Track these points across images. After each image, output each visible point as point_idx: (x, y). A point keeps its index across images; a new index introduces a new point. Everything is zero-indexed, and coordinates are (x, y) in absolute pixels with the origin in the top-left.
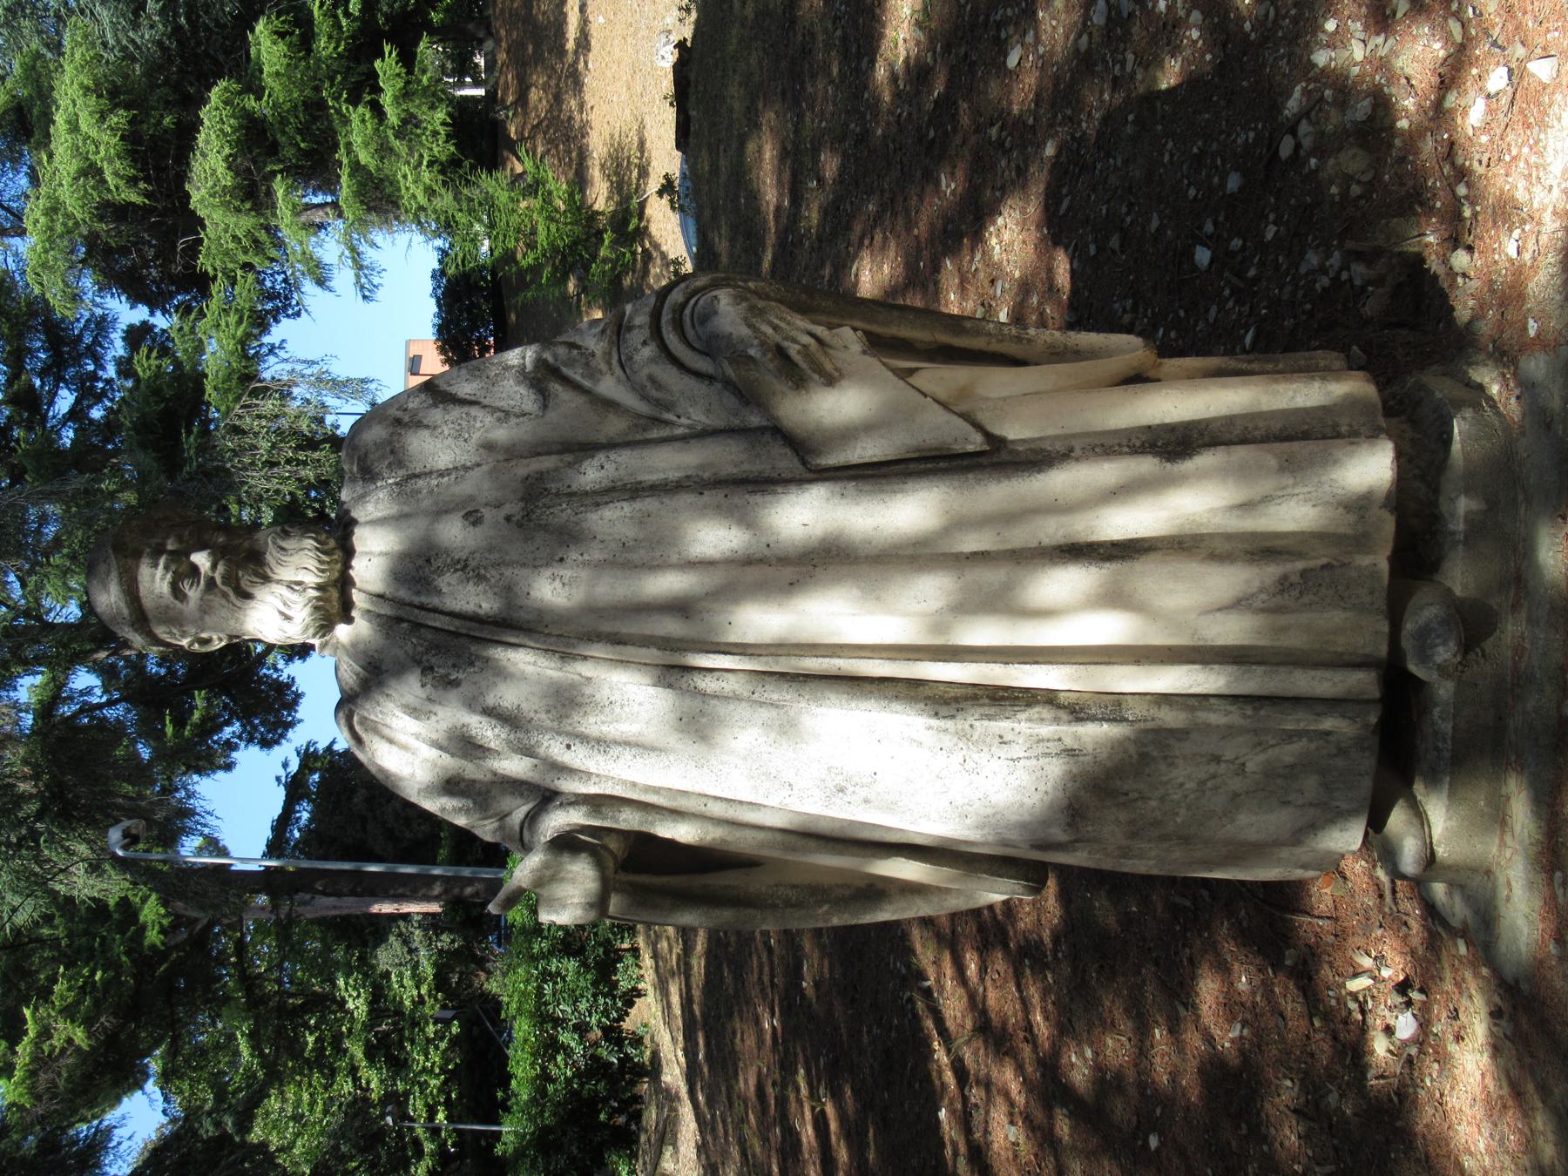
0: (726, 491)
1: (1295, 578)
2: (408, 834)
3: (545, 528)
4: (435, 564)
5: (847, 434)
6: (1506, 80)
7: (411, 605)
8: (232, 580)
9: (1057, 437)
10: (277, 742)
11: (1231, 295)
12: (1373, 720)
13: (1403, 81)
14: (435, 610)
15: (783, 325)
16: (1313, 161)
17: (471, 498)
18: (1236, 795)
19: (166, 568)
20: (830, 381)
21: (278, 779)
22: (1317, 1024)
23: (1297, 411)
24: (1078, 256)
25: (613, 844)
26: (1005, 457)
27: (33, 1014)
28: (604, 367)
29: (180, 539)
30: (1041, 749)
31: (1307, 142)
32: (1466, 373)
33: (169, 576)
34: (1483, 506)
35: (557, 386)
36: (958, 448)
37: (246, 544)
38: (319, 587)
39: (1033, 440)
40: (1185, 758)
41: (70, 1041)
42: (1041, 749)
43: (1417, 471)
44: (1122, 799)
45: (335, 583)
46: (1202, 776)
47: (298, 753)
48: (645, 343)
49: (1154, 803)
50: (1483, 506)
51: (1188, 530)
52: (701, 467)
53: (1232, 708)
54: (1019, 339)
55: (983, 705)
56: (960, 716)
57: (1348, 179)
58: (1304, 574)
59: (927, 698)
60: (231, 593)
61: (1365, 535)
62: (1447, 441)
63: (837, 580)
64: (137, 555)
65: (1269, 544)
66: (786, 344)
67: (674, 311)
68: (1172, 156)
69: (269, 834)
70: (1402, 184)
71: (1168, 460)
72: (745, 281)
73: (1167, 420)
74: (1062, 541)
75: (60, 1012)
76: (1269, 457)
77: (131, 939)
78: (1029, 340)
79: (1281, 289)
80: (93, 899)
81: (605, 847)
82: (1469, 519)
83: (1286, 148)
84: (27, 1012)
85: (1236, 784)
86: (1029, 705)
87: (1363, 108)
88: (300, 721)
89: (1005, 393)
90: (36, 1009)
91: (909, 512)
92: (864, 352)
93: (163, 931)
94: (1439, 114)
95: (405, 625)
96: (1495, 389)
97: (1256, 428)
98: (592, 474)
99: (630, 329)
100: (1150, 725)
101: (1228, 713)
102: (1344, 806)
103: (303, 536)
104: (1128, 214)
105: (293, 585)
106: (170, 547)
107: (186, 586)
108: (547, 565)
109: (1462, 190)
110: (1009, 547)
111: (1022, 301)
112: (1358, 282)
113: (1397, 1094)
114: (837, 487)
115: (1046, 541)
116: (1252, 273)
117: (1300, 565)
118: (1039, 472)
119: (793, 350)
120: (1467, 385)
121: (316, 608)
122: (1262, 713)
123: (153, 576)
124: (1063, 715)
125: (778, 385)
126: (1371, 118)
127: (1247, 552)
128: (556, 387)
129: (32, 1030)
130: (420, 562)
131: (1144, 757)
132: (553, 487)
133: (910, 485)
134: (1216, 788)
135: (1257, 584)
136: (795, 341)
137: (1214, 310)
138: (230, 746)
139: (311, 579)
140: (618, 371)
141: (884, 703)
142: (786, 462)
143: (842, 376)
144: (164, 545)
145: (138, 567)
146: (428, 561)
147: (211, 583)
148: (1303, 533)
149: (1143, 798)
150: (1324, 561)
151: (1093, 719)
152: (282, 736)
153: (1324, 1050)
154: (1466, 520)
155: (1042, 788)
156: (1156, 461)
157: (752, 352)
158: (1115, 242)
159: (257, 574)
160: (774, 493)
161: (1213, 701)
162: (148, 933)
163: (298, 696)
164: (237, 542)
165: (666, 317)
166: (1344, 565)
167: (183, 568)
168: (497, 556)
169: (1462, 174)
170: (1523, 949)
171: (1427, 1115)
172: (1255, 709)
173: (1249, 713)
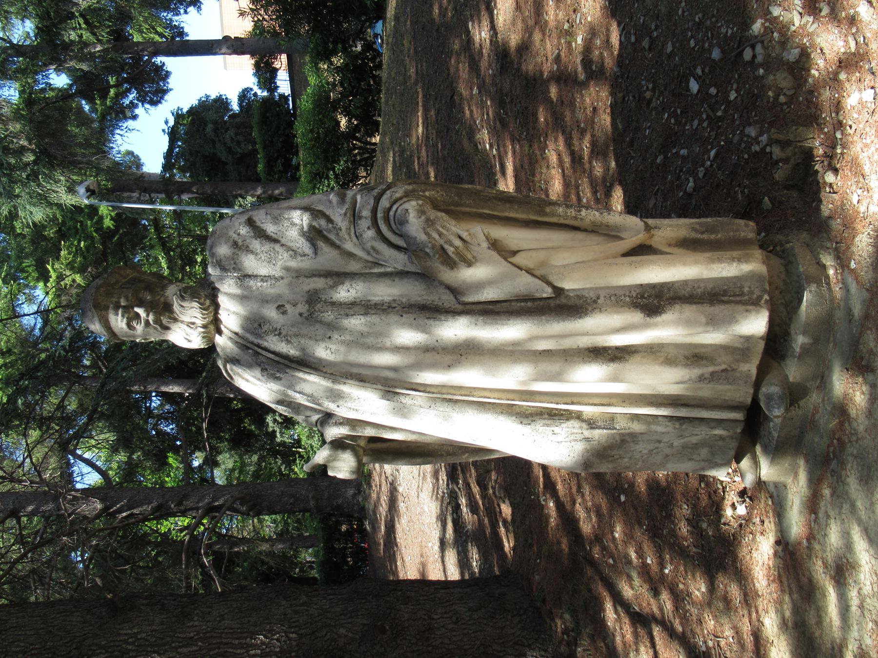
0: (415, 316)
1: (707, 376)
2: (239, 150)
3: (321, 322)
4: (265, 328)
5: (479, 286)
6: (872, 97)
7: (252, 343)
8: (157, 321)
9: (591, 289)
10: (160, 102)
11: (707, 119)
12: (739, 431)
13: (819, 51)
14: (266, 349)
15: (444, 232)
16: (761, 71)
17: (279, 296)
18: (667, 456)
19: (123, 316)
20: (469, 264)
21: (164, 131)
22: (703, 485)
23: (722, 279)
24: (624, 32)
25: (362, 443)
26: (563, 301)
27: (52, 267)
28: (346, 237)
29: (127, 299)
30: (573, 437)
31: (760, 59)
32: (819, 253)
33: (125, 320)
34: (811, 341)
35: (322, 244)
36: (538, 295)
37: (162, 299)
38: (204, 326)
39: (579, 290)
40: (643, 441)
41: (74, 281)
42: (573, 437)
43: (783, 301)
44: (610, 459)
45: (212, 322)
46: (652, 448)
47: (173, 114)
48: (369, 228)
49: (626, 460)
50: (811, 341)
51: (656, 341)
52: (401, 296)
53: (669, 424)
54: (576, 218)
55: (545, 419)
56: (533, 424)
57: (779, 91)
58: (712, 374)
59: (517, 414)
60: (158, 327)
61: (748, 349)
62: (800, 300)
63: (473, 364)
64: (106, 308)
65: (697, 351)
66: (446, 247)
67: (384, 212)
68: (684, 12)
69: (163, 160)
70: (809, 107)
71: (648, 316)
72: (424, 191)
73: (651, 282)
74: (590, 346)
75: (67, 266)
76: (702, 317)
77: (97, 223)
78: (582, 219)
79: (733, 136)
80: (72, 205)
81: (359, 446)
82: (802, 347)
83: (747, 55)
84: (49, 267)
85: (668, 451)
86: (568, 420)
87: (793, 55)
88: (171, 90)
89: (565, 263)
90: (53, 264)
91: (511, 331)
92: (489, 248)
93: (112, 219)
94: (833, 80)
95: (251, 351)
96: (831, 272)
97: (699, 287)
98: (345, 293)
99: (360, 218)
100: (627, 431)
101: (667, 426)
102: (719, 462)
103: (192, 300)
104: (656, 30)
105: (191, 324)
106: (123, 304)
107: (134, 324)
108: (323, 340)
109: (838, 135)
110: (562, 348)
111: (591, 39)
112: (774, 157)
113: (733, 535)
114: (473, 320)
115: (581, 346)
116: (719, 114)
117: (711, 369)
118: (580, 318)
119: (450, 250)
120: (818, 263)
121: (203, 337)
122: (684, 427)
123: (117, 320)
124: (584, 425)
125: (442, 268)
126: (798, 61)
127: (687, 358)
128: (321, 244)
129: (53, 275)
130: (256, 325)
131: (623, 441)
132: (323, 297)
133: (511, 322)
134: (658, 453)
135: (688, 377)
136: (451, 245)
137: (696, 123)
138: (133, 106)
139: (199, 322)
140: (355, 239)
141: (495, 416)
142: (447, 299)
143: (476, 260)
144: (119, 302)
145: (108, 314)
146: (260, 325)
147: (147, 323)
148: (716, 345)
149: (621, 458)
150: (724, 367)
151: (599, 428)
152: (162, 98)
153: (704, 501)
154: (801, 347)
155: (572, 455)
156: (642, 315)
157: (427, 250)
158: (646, 43)
159: (170, 318)
160: (440, 320)
161: (660, 419)
162: (105, 221)
163: (168, 74)
164: (157, 298)
165: (380, 215)
166: (733, 370)
167: (132, 314)
168: (296, 330)
169: (840, 125)
170: (793, 534)
171: (743, 552)
172: (680, 424)
173: (677, 426)
